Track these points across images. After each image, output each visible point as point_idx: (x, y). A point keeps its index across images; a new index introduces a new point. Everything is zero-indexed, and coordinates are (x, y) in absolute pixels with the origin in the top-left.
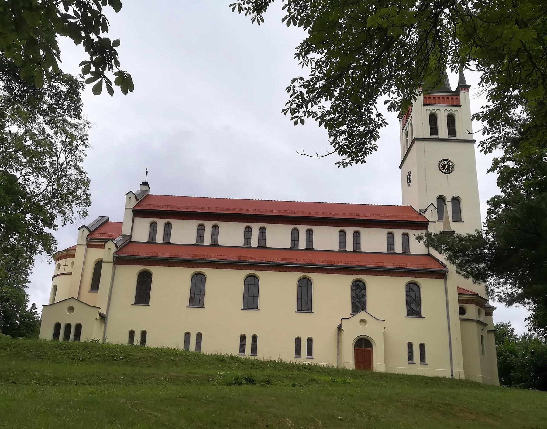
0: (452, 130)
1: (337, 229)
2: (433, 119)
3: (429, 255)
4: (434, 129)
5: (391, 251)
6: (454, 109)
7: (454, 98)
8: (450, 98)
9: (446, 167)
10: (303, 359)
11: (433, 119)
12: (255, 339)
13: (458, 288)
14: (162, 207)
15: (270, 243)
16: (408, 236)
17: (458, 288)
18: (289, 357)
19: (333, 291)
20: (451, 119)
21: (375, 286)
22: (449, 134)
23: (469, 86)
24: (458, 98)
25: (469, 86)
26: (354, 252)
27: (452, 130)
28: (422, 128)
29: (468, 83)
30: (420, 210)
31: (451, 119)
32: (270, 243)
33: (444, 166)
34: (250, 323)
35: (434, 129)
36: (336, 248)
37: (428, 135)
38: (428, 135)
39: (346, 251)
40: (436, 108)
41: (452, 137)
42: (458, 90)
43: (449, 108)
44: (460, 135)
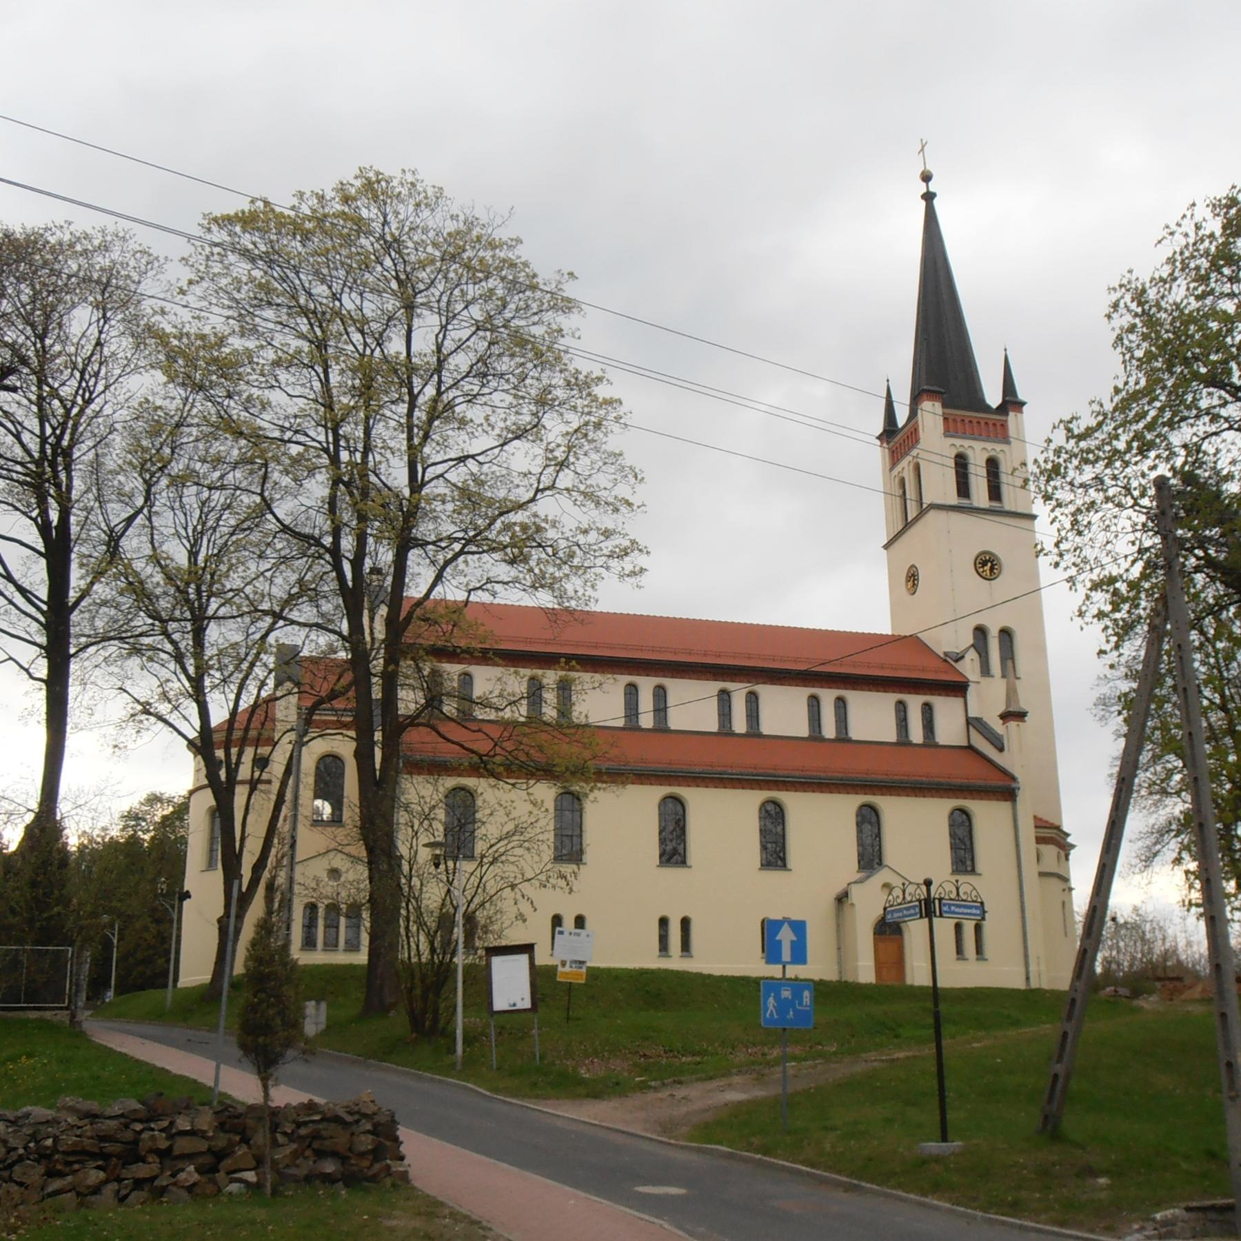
0: (995, 492)
1: (714, 686)
2: (961, 463)
3: (970, 748)
4: (963, 488)
5: (725, 730)
6: (999, 447)
7: (998, 424)
8: (982, 422)
9: (987, 565)
10: (675, 962)
11: (961, 463)
12: (685, 923)
13: (1035, 817)
14: (547, 643)
15: (678, 720)
16: (757, 698)
17: (1035, 817)
18: (650, 960)
19: (723, 820)
20: (993, 465)
21: (897, 813)
22: (991, 499)
23: (1023, 404)
24: (1004, 426)
25: (1023, 404)
26: (924, 745)
27: (995, 492)
28: (940, 486)
29: (1021, 396)
30: (946, 654)
31: (993, 465)
32: (678, 720)
33: (984, 564)
34: (673, 892)
35: (963, 488)
36: (713, 726)
37: (953, 499)
38: (953, 499)
39: (910, 744)
40: (967, 443)
41: (964, 502)
42: (1003, 409)
43: (989, 446)
44: (1008, 503)
